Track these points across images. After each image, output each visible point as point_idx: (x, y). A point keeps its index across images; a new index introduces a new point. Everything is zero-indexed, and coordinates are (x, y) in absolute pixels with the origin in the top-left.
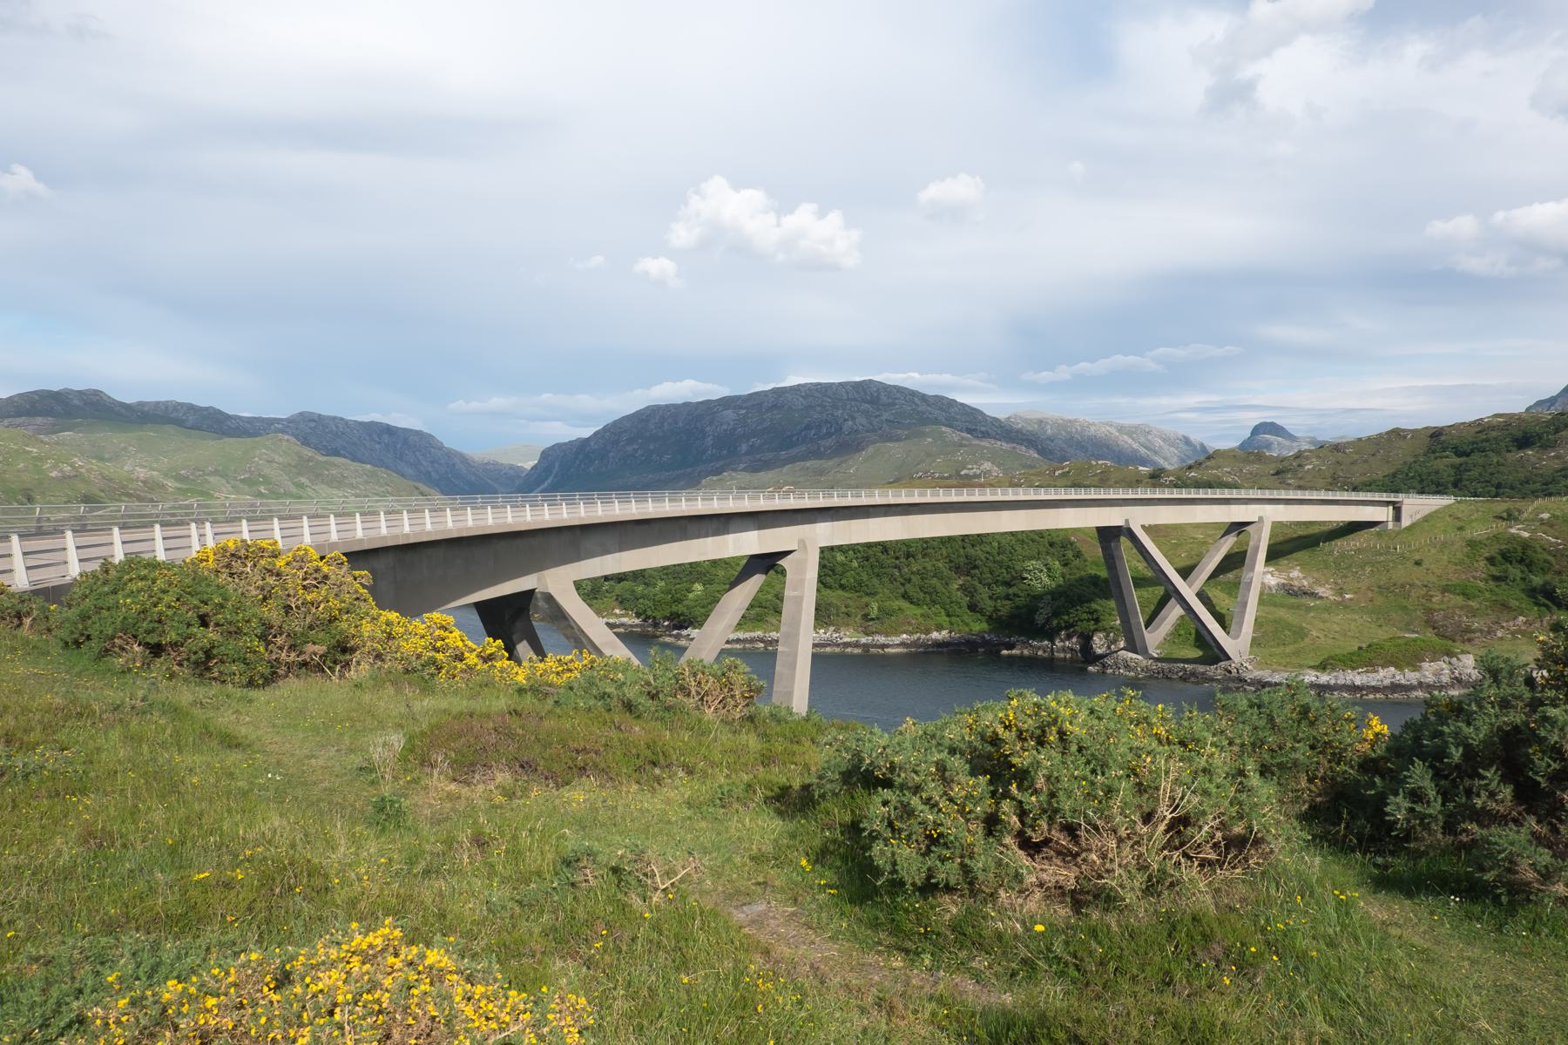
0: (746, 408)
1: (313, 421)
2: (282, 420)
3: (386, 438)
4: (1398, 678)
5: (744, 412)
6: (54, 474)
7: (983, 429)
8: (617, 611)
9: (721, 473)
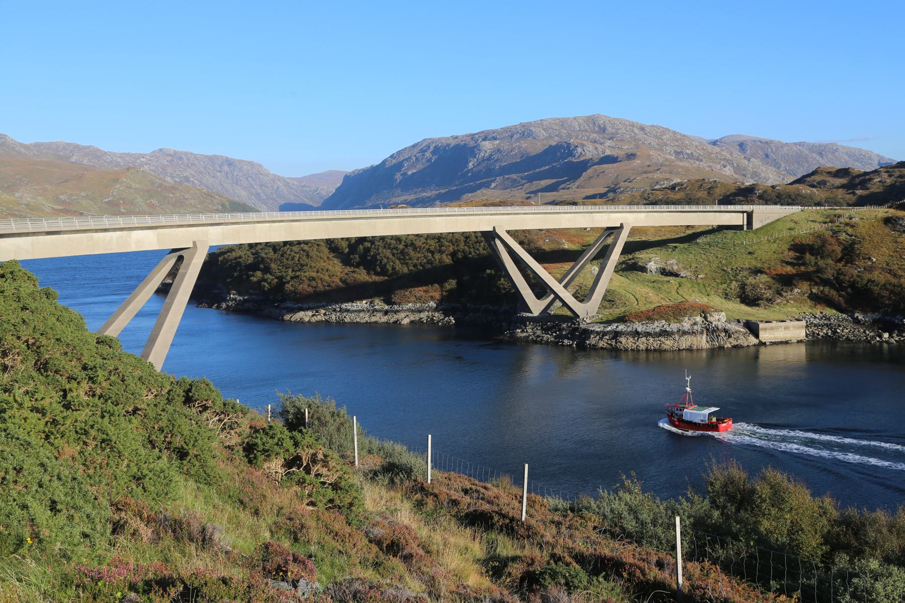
1: (170, 155)
2: (146, 155)
3: (226, 168)
5: (497, 142)
7: (689, 152)
9: (476, 191)
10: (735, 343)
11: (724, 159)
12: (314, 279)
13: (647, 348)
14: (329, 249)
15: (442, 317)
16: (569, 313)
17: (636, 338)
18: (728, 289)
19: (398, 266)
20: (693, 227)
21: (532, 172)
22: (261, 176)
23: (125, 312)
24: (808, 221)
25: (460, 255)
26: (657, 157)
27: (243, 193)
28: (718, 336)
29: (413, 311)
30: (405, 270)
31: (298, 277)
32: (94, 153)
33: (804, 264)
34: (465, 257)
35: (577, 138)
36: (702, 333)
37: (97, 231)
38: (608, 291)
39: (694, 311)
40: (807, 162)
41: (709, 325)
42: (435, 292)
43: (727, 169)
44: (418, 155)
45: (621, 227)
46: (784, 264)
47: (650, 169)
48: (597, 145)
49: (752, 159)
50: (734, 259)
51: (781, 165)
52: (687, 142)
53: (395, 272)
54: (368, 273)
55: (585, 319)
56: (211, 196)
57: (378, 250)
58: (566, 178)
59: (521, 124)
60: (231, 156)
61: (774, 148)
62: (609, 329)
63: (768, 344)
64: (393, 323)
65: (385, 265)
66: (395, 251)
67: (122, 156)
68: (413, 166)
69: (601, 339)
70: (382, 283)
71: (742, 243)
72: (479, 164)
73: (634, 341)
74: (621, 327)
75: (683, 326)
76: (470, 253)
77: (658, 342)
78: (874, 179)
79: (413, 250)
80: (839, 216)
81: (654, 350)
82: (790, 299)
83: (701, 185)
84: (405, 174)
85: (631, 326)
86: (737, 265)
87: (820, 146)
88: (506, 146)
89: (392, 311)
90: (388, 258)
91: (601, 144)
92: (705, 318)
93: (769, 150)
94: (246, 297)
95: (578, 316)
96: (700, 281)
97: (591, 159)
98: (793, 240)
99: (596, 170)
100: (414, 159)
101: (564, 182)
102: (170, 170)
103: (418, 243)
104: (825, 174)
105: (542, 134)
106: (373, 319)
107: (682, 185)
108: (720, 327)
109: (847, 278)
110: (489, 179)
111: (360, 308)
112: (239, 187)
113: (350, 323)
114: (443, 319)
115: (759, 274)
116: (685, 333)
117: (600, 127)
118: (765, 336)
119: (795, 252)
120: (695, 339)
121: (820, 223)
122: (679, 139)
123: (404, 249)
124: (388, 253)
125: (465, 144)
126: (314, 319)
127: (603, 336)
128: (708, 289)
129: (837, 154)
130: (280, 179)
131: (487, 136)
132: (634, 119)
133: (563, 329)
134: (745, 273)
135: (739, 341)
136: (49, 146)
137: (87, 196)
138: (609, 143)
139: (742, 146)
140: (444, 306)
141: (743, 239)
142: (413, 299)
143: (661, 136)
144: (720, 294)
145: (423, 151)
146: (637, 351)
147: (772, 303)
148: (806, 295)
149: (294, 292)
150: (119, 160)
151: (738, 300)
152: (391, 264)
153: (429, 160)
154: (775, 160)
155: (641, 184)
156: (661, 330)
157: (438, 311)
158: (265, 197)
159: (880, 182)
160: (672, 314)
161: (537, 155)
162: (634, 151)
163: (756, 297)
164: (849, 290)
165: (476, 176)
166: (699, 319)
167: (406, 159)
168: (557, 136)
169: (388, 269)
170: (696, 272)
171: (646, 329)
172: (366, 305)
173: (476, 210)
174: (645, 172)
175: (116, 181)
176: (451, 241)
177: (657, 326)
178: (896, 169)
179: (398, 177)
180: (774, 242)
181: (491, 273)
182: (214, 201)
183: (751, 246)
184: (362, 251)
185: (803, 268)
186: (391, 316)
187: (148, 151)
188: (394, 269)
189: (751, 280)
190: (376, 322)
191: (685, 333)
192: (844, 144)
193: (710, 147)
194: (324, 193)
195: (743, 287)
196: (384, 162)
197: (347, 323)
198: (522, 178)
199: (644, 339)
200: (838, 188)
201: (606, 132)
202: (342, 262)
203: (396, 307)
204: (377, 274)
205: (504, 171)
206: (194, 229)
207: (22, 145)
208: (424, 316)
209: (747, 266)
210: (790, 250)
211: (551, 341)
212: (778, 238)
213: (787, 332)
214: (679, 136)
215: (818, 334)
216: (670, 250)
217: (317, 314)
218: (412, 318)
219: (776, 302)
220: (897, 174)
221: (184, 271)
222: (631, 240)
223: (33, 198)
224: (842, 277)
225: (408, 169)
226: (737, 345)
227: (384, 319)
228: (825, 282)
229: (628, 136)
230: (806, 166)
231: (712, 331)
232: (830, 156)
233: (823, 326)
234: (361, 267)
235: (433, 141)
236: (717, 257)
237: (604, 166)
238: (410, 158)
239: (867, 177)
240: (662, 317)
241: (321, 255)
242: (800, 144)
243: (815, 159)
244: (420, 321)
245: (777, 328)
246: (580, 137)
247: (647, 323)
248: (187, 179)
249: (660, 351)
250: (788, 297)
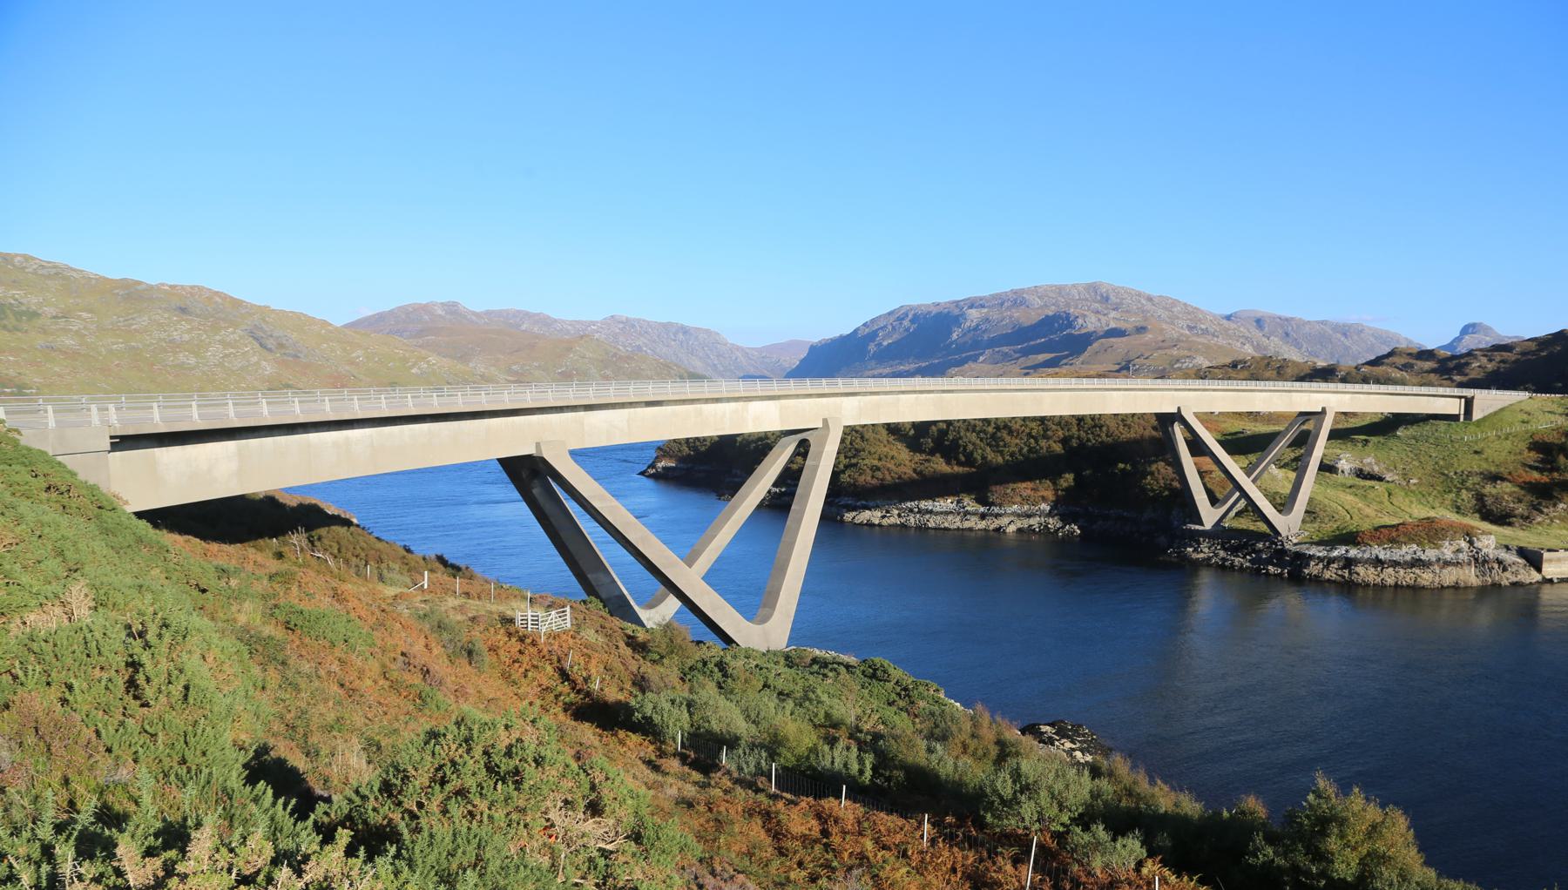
0: (989, 307)
1: (622, 322)
2: (597, 322)
4: (1418, 554)
5: (986, 310)
6: (414, 371)
7: (1203, 327)
8: (789, 481)
9: (963, 365)
10: (1514, 579)
11: (1243, 336)
12: (878, 469)
13: (1396, 583)
14: (887, 430)
16: (1263, 527)
17: (1379, 569)
18: (1459, 501)
19: (990, 455)
20: (1354, 414)
21: (1026, 344)
22: (719, 346)
24: (1544, 412)
25: (1074, 443)
26: (1172, 332)
28: (1491, 569)
29: (1019, 516)
30: (1000, 459)
31: (855, 465)
34: (1082, 445)
35: (1076, 307)
37: (707, 401)
38: (1311, 500)
39: (1455, 532)
40: (1331, 343)
41: (1477, 553)
42: (1047, 490)
43: (1246, 347)
44: (894, 323)
45: (1324, 412)
46: (1527, 469)
48: (1100, 317)
49: (1272, 338)
51: (1302, 346)
52: (1201, 316)
53: (986, 462)
55: (1290, 538)
56: (668, 367)
57: (959, 433)
58: (1066, 353)
59: (1012, 290)
60: (686, 323)
61: (1295, 326)
62: (1335, 553)
63: (1556, 581)
64: (993, 530)
65: (972, 453)
66: (982, 435)
67: (572, 323)
68: (888, 335)
69: (1327, 567)
70: (969, 475)
72: (964, 335)
73: (1376, 573)
74: (1353, 552)
75: (1442, 553)
76: (1089, 440)
77: (1412, 575)
78: (1471, 363)
79: (1009, 434)
81: (1408, 586)
82: (1555, 516)
83: (1269, 364)
84: (880, 344)
85: (1368, 551)
86: (1461, 469)
87: (1344, 326)
89: (991, 515)
90: (974, 444)
91: (1105, 315)
92: (1471, 543)
93: (1290, 328)
94: (783, 490)
96: (1414, 488)
97: (1095, 332)
98: (1531, 436)
100: (890, 327)
101: (1066, 357)
102: (622, 339)
103: (1015, 427)
104: (1404, 356)
105: (1037, 302)
106: (967, 525)
107: (1245, 363)
110: (977, 352)
111: (945, 509)
112: (694, 358)
113: (935, 529)
115: (1499, 482)
116: (1447, 563)
117: (1102, 296)
118: (1550, 570)
119: (1538, 452)
120: (1461, 571)
121: (1561, 415)
122: (1193, 316)
123: (995, 433)
124: (973, 437)
125: (949, 312)
127: (1329, 563)
128: (1430, 499)
129: (1362, 335)
130: (738, 348)
131: (973, 303)
133: (1260, 551)
134: (1477, 479)
135: (1519, 577)
136: (499, 313)
137: (539, 366)
138: (1113, 314)
139: (1259, 322)
140: (1064, 507)
142: (1018, 499)
143: (1172, 307)
144: (1449, 507)
145: (900, 319)
146: (1381, 587)
147: (1530, 522)
150: (569, 327)
151: (1477, 515)
153: (907, 330)
154: (1296, 340)
155: (1158, 359)
156: (1413, 558)
157: (1053, 517)
158: (722, 369)
159: (1479, 367)
160: (1425, 537)
161: (1031, 326)
162: (1143, 324)
163: (1504, 513)
165: (961, 348)
166: (1464, 545)
167: (881, 328)
168: (1054, 305)
171: (1391, 556)
174: (1160, 348)
175: (569, 349)
176: (1059, 424)
177: (1406, 552)
178: (1496, 353)
179: (872, 347)
180: (1507, 439)
181: (1124, 469)
182: (672, 371)
183: (1476, 443)
184: (936, 434)
185: (1556, 475)
186: (990, 521)
187: (598, 317)
188: (984, 458)
189: (1489, 489)
190: (970, 529)
191: (1447, 563)
192: (1371, 325)
193: (1225, 322)
195: (1480, 497)
196: (856, 331)
197: (931, 529)
198: (1015, 352)
199: (1391, 570)
200: (1427, 372)
201: (1110, 302)
202: (907, 447)
203: (996, 510)
204: (960, 464)
205: (993, 343)
206: (824, 400)
207: (474, 313)
208: (1034, 521)
210: (1530, 449)
211: (1247, 567)
212: (1510, 434)
214: (1191, 310)
216: (1360, 445)
217: (888, 515)
218: (1019, 525)
219: (1536, 521)
220: (1498, 359)
222: (1335, 427)
223: (486, 369)
225: (883, 339)
226: (1517, 582)
227: (982, 525)
229: (1135, 307)
230: (1330, 346)
231: (1480, 562)
232: (1355, 337)
234: (938, 455)
235: (911, 308)
236: (1431, 456)
238: (885, 326)
240: (1412, 540)
241: (878, 436)
242: (1323, 323)
243: (1340, 340)
244: (1030, 529)
246: (1080, 306)
247: (1390, 548)
248: (639, 348)
249: (1415, 589)
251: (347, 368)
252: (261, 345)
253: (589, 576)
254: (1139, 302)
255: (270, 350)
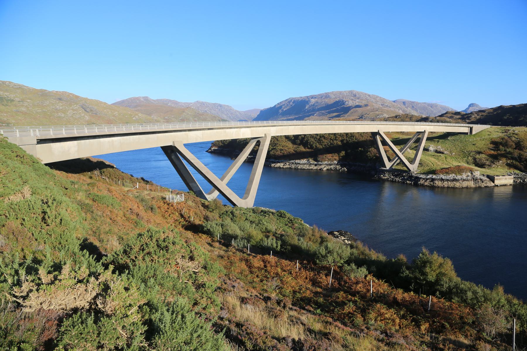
1: (200, 103)
2: (192, 103)
3: (219, 107)
4: (455, 177)
5: (317, 99)
7: (386, 104)
10: (486, 185)
11: (399, 108)
12: (282, 150)
13: (448, 186)
15: (340, 168)
16: (405, 169)
17: (442, 182)
19: (318, 145)
23: (235, 167)
26: (376, 106)
27: (225, 116)
28: (478, 182)
29: (327, 165)
30: (321, 147)
31: (275, 149)
32: (176, 103)
33: (499, 150)
34: (347, 142)
36: (471, 180)
37: (228, 128)
38: (421, 160)
42: (336, 157)
45: (425, 132)
47: (374, 110)
48: (353, 101)
49: (408, 108)
50: (467, 147)
54: (305, 148)
57: (308, 138)
62: (428, 177)
65: (312, 145)
66: (315, 139)
67: (185, 103)
68: (286, 107)
69: (426, 181)
70: (311, 152)
71: (469, 140)
74: (434, 177)
76: (350, 141)
80: (509, 130)
84: (283, 110)
85: (439, 176)
86: (469, 150)
88: (319, 101)
89: (318, 165)
90: (313, 142)
91: (355, 101)
92: (472, 173)
95: (410, 170)
96: (453, 156)
99: (354, 110)
102: (200, 108)
103: (326, 136)
105: (333, 97)
106: (311, 168)
108: (478, 178)
109: (524, 157)
111: (303, 163)
114: (341, 169)
116: (464, 180)
117: (354, 94)
118: (497, 182)
121: (501, 133)
122: (383, 100)
123: (320, 138)
124: (313, 140)
126: (285, 167)
127: (426, 180)
130: (238, 111)
131: (312, 97)
132: (366, 92)
135: (487, 184)
137: (174, 117)
138: (357, 100)
139: (404, 103)
140: (342, 162)
141: (467, 138)
142: (327, 159)
145: (289, 102)
146: (443, 188)
148: (505, 164)
149: (275, 155)
150: (184, 105)
152: (315, 144)
157: (338, 165)
162: (367, 104)
164: (525, 162)
165: (309, 111)
166: (469, 174)
167: (283, 105)
169: (314, 147)
170: (451, 152)
172: (306, 162)
173: (348, 122)
174: (372, 111)
175: (184, 112)
177: (451, 176)
179: (280, 111)
180: (483, 140)
181: (361, 150)
185: (499, 152)
187: (193, 102)
188: (316, 146)
189: (477, 156)
190: (312, 169)
191: (464, 180)
192: (440, 104)
193: (393, 103)
194: (253, 117)
195: (475, 159)
196: (275, 106)
199: (446, 182)
202: (292, 143)
203: (320, 163)
204: (308, 148)
205: (319, 110)
207: (153, 100)
208: (332, 167)
209: (473, 150)
210: (491, 144)
211: (400, 181)
213: (506, 180)
215: (517, 182)
216: (436, 142)
221: (262, 148)
224: (522, 157)
225: (284, 108)
227: (315, 168)
228: (513, 158)
231: (475, 180)
232: (435, 108)
233: (518, 178)
234: (301, 145)
235: (293, 98)
237: (357, 109)
238: (285, 104)
239: (469, 115)
240: (453, 173)
243: (430, 109)
244: (331, 169)
245: (502, 179)
248: (206, 111)
249: (454, 188)
250: (498, 164)
251: (112, 118)
252: (85, 110)
253: (190, 184)
254: (366, 96)
255: (88, 112)
